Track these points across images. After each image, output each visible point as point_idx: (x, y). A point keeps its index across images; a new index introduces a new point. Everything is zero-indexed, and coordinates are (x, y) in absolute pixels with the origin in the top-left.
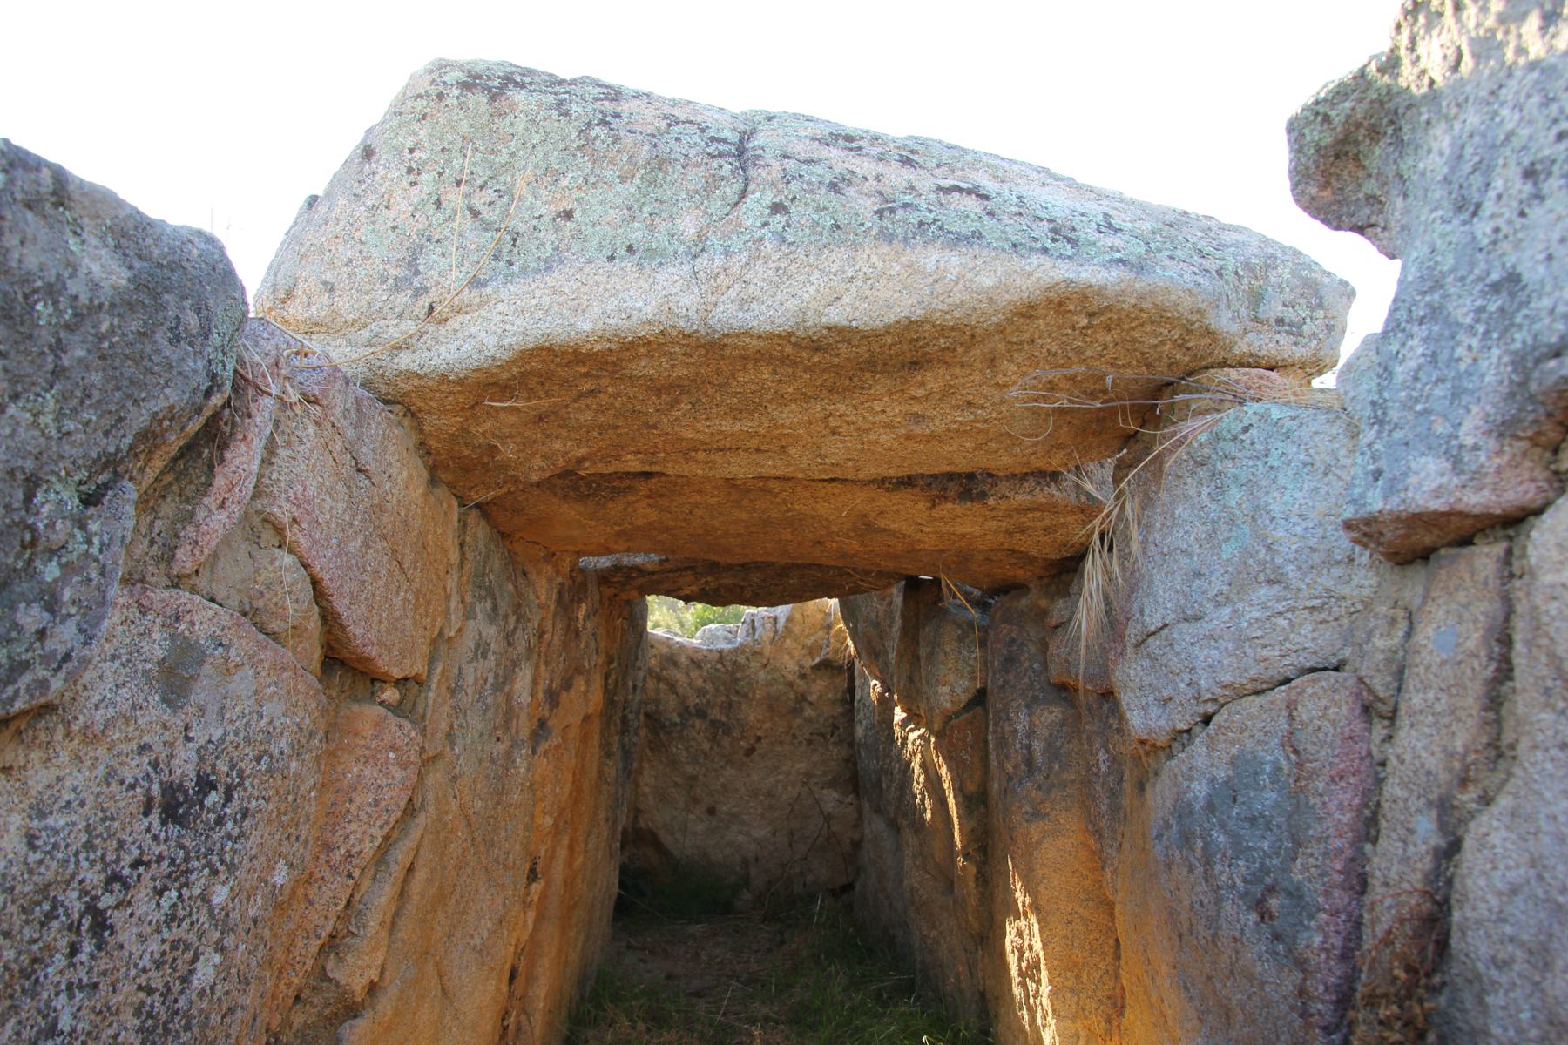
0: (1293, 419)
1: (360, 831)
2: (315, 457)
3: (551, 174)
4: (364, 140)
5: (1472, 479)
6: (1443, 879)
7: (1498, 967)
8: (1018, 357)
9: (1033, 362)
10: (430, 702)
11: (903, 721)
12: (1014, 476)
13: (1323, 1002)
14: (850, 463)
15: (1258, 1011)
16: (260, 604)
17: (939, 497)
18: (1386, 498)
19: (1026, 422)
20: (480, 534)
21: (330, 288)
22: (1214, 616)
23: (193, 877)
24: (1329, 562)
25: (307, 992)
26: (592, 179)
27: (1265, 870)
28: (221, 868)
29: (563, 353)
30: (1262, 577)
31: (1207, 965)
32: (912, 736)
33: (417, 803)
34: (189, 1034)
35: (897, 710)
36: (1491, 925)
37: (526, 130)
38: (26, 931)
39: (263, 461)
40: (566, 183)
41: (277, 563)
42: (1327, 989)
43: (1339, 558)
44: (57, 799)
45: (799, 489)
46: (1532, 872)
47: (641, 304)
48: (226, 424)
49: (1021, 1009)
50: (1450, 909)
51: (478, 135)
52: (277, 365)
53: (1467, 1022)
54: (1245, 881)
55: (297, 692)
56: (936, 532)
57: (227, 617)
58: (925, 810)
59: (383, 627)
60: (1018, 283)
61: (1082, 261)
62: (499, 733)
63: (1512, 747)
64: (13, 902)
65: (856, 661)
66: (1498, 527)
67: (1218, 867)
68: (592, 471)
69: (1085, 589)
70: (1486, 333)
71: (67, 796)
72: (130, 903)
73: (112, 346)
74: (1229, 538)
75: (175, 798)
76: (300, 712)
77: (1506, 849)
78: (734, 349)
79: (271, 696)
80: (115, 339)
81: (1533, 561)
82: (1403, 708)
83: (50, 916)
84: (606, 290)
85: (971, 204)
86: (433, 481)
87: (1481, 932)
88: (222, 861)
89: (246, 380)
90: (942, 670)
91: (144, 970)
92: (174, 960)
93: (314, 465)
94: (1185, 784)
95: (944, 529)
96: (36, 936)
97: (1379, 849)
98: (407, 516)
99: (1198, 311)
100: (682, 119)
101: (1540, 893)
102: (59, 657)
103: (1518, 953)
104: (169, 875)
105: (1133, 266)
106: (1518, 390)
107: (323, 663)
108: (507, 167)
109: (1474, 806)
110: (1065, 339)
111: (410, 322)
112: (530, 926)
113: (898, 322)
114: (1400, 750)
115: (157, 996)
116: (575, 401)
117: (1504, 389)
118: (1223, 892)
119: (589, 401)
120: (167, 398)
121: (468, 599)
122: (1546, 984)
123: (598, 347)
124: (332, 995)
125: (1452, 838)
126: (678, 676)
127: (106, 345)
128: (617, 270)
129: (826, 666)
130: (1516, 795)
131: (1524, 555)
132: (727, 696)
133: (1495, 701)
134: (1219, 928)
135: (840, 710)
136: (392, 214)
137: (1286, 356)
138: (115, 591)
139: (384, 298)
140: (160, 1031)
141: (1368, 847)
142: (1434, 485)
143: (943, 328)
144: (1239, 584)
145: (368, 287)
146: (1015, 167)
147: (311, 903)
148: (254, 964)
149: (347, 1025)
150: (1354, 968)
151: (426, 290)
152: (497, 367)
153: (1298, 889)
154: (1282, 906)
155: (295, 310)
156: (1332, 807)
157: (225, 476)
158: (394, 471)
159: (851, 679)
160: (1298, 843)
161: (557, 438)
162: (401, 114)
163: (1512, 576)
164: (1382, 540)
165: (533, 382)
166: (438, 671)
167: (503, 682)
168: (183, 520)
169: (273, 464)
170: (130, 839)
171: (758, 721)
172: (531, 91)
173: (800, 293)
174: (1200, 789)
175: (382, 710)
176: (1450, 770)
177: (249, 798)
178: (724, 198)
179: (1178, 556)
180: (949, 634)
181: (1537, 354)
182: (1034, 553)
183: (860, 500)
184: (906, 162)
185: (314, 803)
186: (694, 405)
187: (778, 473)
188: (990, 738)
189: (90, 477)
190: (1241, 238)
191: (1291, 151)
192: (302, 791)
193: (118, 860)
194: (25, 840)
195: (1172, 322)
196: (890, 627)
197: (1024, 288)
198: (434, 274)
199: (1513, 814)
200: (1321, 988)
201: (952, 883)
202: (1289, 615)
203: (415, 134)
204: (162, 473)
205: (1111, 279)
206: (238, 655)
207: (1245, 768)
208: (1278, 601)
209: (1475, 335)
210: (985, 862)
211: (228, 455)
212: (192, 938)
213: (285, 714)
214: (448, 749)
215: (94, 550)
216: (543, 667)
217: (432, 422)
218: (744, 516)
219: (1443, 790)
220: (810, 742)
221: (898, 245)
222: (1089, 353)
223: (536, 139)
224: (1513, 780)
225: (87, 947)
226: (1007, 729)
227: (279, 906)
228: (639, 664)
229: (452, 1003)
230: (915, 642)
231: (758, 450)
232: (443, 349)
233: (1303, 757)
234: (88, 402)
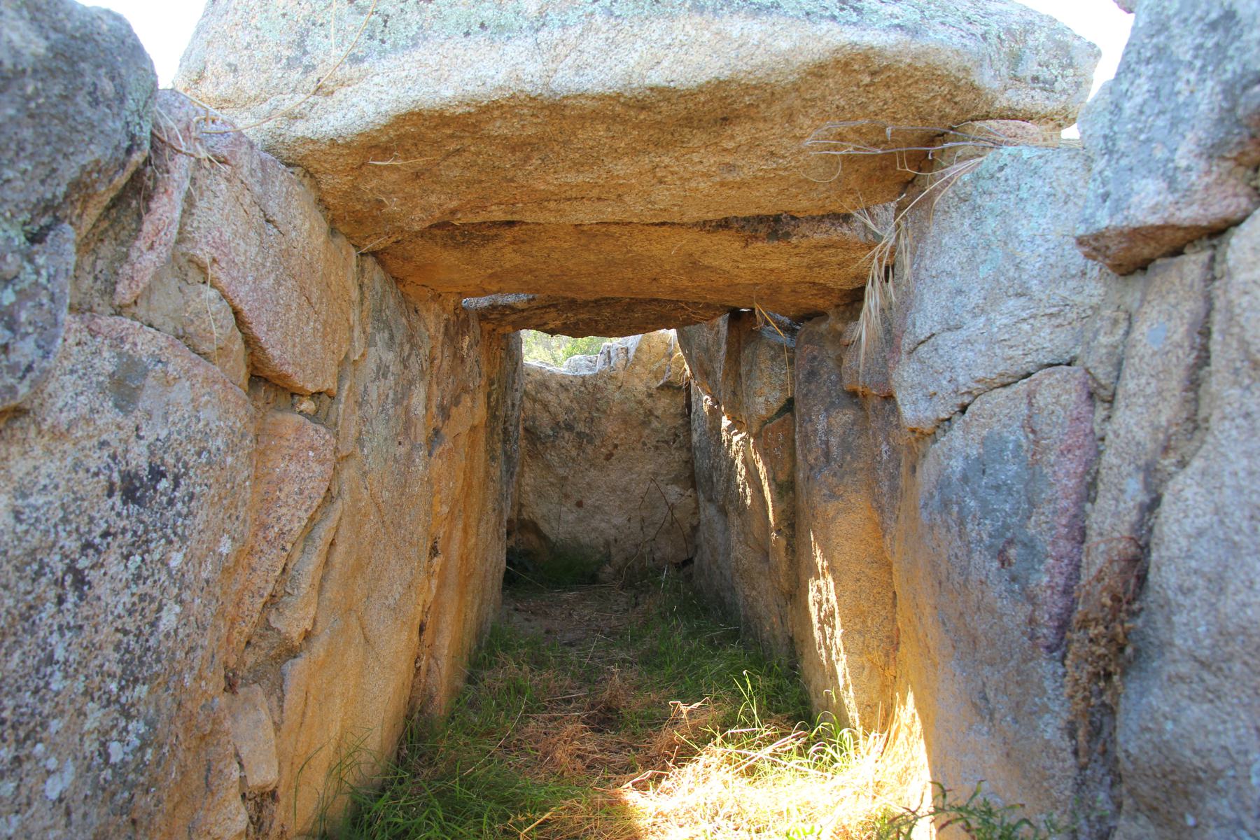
0: (1040, 157)
2: (228, 208)
5: (1184, 196)
6: (1145, 528)
7: (1184, 594)
9: (825, 116)
10: (341, 412)
12: (813, 218)
13: (1047, 627)
16: (191, 329)
17: (750, 237)
18: (1111, 216)
19: (821, 170)
20: (376, 277)
21: (234, 69)
23: (153, 546)
24: (1066, 276)
27: (1006, 527)
28: (175, 539)
29: (432, 117)
30: (1011, 292)
32: (736, 439)
33: (335, 492)
35: (724, 419)
36: (1180, 561)
38: (21, 584)
39: (184, 211)
41: (203, 296)
42: (1051, 617)
43: (1074, 272)
44: (35, 484)
45: (636, 231)
46: (1215, 518)
50: (1149, 552)
52: (188, 128)
53: (1157, 637)
54: (990, 536)
56: (750, 268)
59: (297, 350)
60: (810, 46)
63: (1206, 420)
64: (8, 562)
66: (1204, 238)
67: (970, 526)
68: (464, 221)
69: (865, 306)
70: (1203, 68)
71: (43, 481)
72: (102, 565)
73: (38, 106)
75: (133, 484)
76: (232, 418)
77: (1195, 501)
78: (573, 109)
80: (41, 101)
81: (1231, 263)
82: (1120, 393)
83: (39, 574)
84: (463, 61)
86: (333, 232)
87: (1173, 567)
88: (175, 534)
89: (163, 142)
90: (758, 384)
91: (119, 617)
92: (143, 609)
93: (228, 215)
95: (756, 265)
96: (29, 588)
97: (1097, 507)
101: (1221, 534)
102: (23, 368)
103: (1201, 582)
104: (133, 544)
106: (1227, 116)
107: (250, 381)
109: (1173, 469)
110: (851, 95)
113: (709, 82)
114: (1116, 427)
115: (131, 637)
116: (444, 160)
117: (1215, 116)
119: (456, 159)
120: (93, 153)
121: (369, 330)
122: (1220, 605)
123: (459, 111)
124: (275, 640)
125: (1154, 495)
126: (550, 397)
127: (33, 105)
128: (472, 45)
129: (668, 386)
130: (1206, 458)
131: (1224, 261)
133: (1194, 383)
134: (969, 574)
135: (680, 422)
138: (65, 316)
140: (136, 662)
141: (1088, 506)
142: (1152, 203)
143: (747, 87)
144: (992, 299)
145: (265, 67)
147: (254, 570)
148: (209, 614)
149: (289, 663)
150: (1073, 601)
151: (314, 67)
153: (1032, 540)
154: (1018, 555)
155: (207, 89)
156: (1061, 474)
157: (152, 223)
158: (298, 222)
159: (689, 396)
160: (1032, 504)
163: (1214, 279)
164: (1108, 253)
165: (408, 144)
166: (346, 387)
167: (402, 397)
168: (120, 260)
170: (98, 516)
173: (627, 59)
174: (957, 465)
176: (1156, 441)
179: (944, 277)
180: (764, 354)
181: (1244, 81)
182: (831, 285)
183: (686, 241)
187: (617, 218)
189: (32, 219)
192: (238, 480)
193: (90, 532)
194: (12, 515)
199: (1203, 474)
200: (1047, 616)
201: (768, 553)
202: (1031, 321)
204: (98, 220)
207: (993, 447)
208: (1023, 310)
209: (1192, 70)
210: (793, 536)
211: (153, 205)
212: (156, 593)
213: (219, 419)
215: (43, 280)
216: (435, 387)
217: (328, 182)
218: (592, 258)
219: (1149, 457)
220: (657, 448)
221: (708, 15)
222: (872, 108)
224: (1205, 446)
225: (72, 598)
226: (810, 428)
227: (226, 570)
228: (516, 386)
230: (737, 362)
231: (599, 199)
232: (331, 117)
233: (1039, 436)
234: (22, 154)
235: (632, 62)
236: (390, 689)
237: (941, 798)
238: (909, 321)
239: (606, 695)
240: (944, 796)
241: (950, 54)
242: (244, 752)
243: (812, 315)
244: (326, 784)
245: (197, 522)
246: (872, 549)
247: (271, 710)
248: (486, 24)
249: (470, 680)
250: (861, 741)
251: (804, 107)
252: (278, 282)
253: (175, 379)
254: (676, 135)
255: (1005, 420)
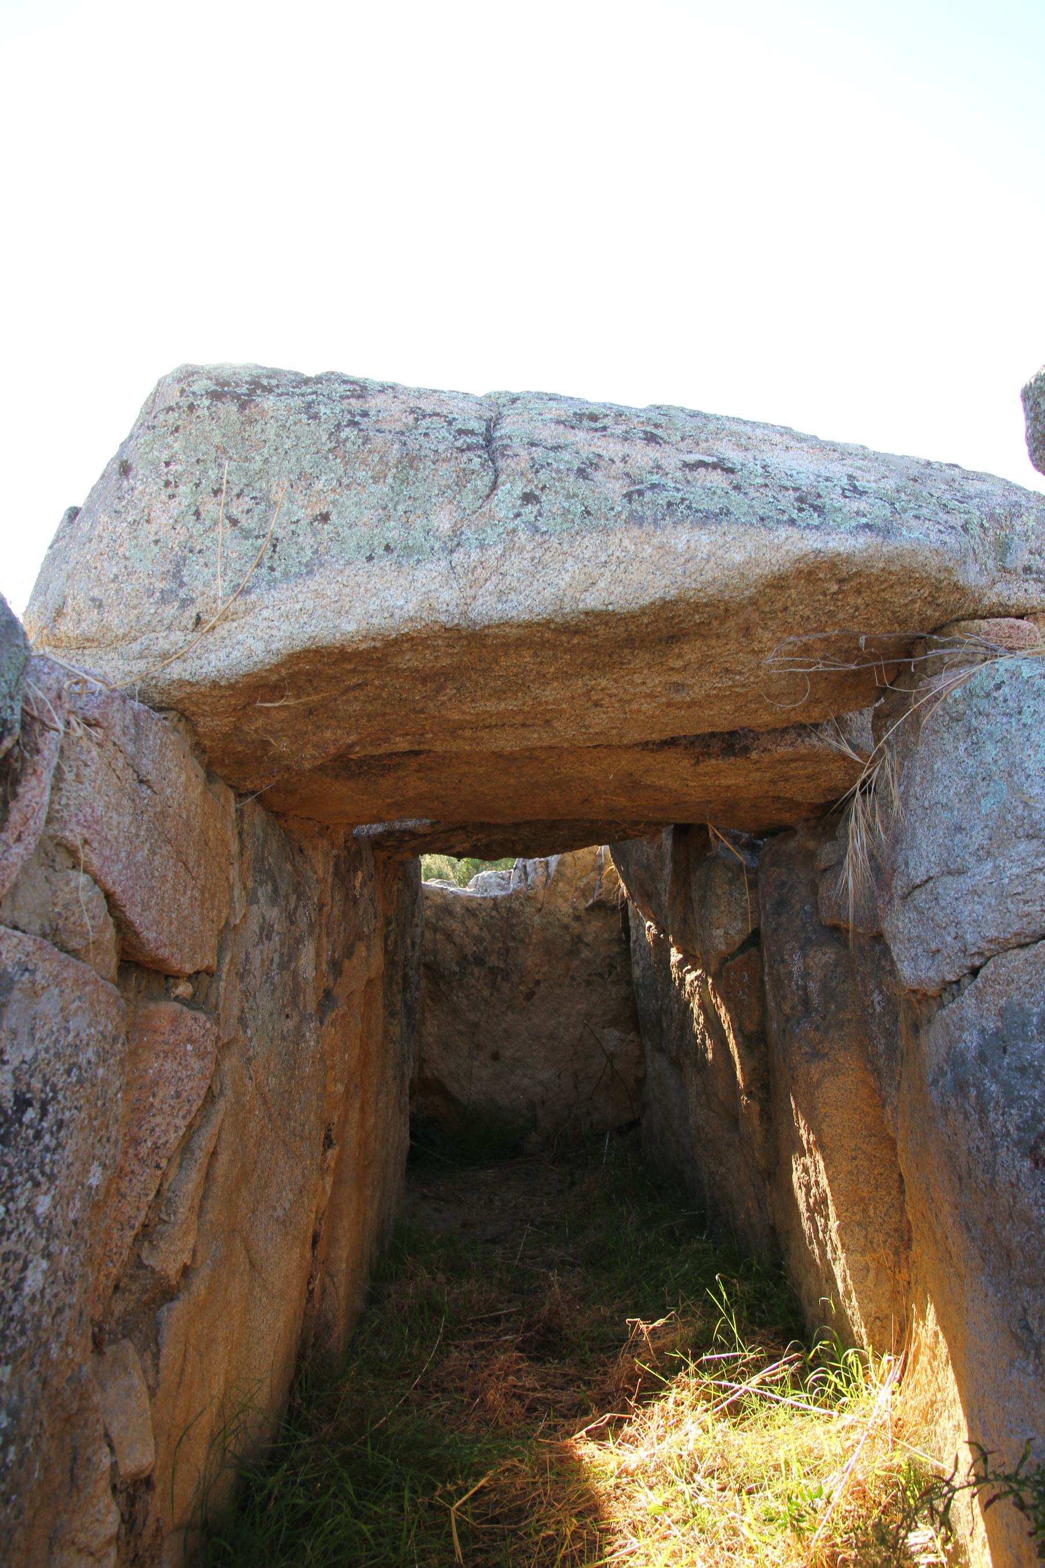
1: (165, 1124)
2: (100, 778)
3: (305, 478)
4: (120, 454)
8: (772, 625)
10: (222, 991)
11: (679, 962)
12: (775, 730)
14: (614, 731)
15: (1036, 1254)
17: (702, 754)
20: (257, 820)
21: (98, 604)
22: (977, 871)
23: (18, 1191)
25: (125, 1280)
26: (345, 481)
28: (42, 1179)
29: (331, 653)
31: (987, 1208)
32: (690, 977)
33: (216, 1090)
34: (24, 1338)
35: (673, 951)
37: (278, 435)
39: (52, 789)
40: (320, 486)
41: (72, 884)
47: (402, 602)
48: (16, 761)
49: (811, 1243)
51: (231, 444)
52: (59, 697)
54: (1018, 1128)
55: (99, 1002)
57: (31, 943)
58: (706, 1050)
59: (173, 928)
60: (768, 556)
61: (829, 530)
62: (288, 1010)
65: (630, 903)
67: (992, 1116)
69: (850, 846)
74: (987, 794)
76: (103, 1021)
79: (76, 1011)
84: (367, 590)
85: (717, 479)
86: (210, 777)
88: (43, 1173)
89: (33, 718)
92: (7, 1270)
93: (100, 787)
94: (957, 1034)
98: (188, 817)
99: (946, 570)
100: (429, 411)
105: (880, 530)
108: (262, 474)
110: (817, 605)
111: (178, 633)
112: (329, 1190)
113: (652, 603)
116: (343, 694)
118: (997, 1139)
121: (250, 884)
123: (363, 646)
126: (455, 925)
128: (376, 570)
129: (600, 906)
132: (504, 942)
134: (995, 1174)
135: (616, 949)
136: (154, 527)
137: (1035, 603)
139: (152, 611)
143: (697, 605)
145: (135, 602)
146: (758, 432)
147: (124, 1196)
148: (77, 1263)
149: (164, 1308)
151: (193, 601)
152: (267, 670)
157: (19, 811)
159: (626, 919)
161: (327, 728)
162: (154, 427)
166: (227, 960)
167: (289, 959)
169: (61, 789)
171: (536, 965)
172: (279, 395)
174: (971, 1039)
175: (177, 1006)
177: (63, 1110)
178: (475, 491)
179: (939, 809)
182: (799, 798)
184: (651, 438)
185: (121, 1104)
186: (458, 690)
188: (766, 979)
190: (985, 487)
191: (1027, 419)
195: (921, 582)
196: (662, 869)
197: (774, 561)
198: (199, 585)
201: (737, 1120)
203: (170, 447)
205: (858, 546)
206: (43, 977)
211: (20, 790)
212: (21, 1248)
213: (89, 1026)
214: (241, 1032)
216: (325, 939)
217: (205, 724)
218: (512, 781)
220: (588, 983)
221: (649, 527)
222: (841, 616)
223: (288, 444)
226: (782, 971)
228: (416, 920)
229: (260, 1275)
231: (523, 725)
232: (212, 657)
235: (562, 584)
236: (281, 1324)
237: (980, 1462)
238: (900, 859)
239: (545, 1311)
240: (985, 1461)
241: (928, 554)
242: (115, 1431)
243: (778, 831)
244: (208, 1457)
245: (66, 1153)
246: (868, 1120)
247: (144, 1371)
248: (392, 546)
249: (373, 1299)
250: (871, 1364)
251: (763, 619)
252: (152, 852)
253: (43, 988)
254: (615, 656)
255: (1026, 988)
